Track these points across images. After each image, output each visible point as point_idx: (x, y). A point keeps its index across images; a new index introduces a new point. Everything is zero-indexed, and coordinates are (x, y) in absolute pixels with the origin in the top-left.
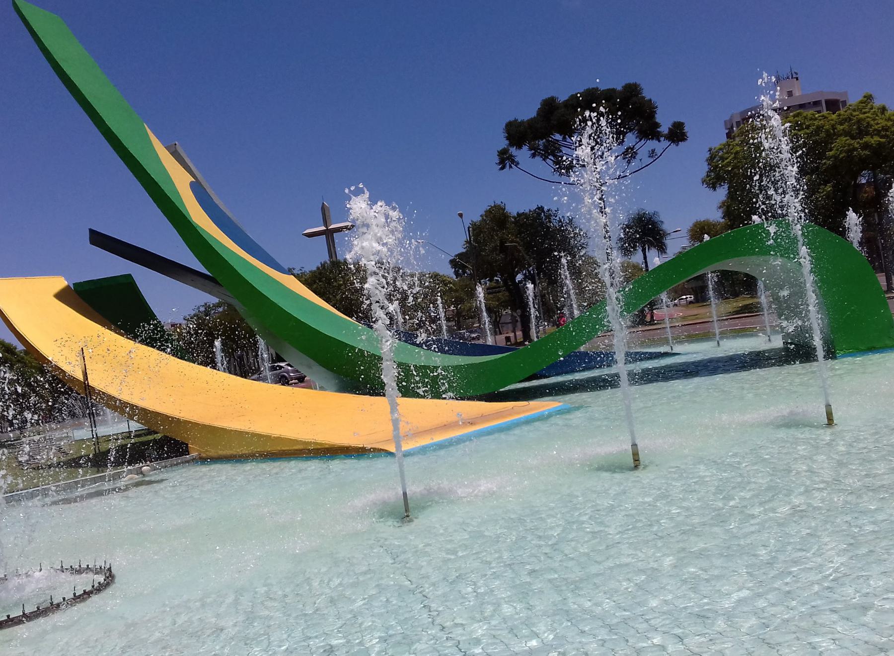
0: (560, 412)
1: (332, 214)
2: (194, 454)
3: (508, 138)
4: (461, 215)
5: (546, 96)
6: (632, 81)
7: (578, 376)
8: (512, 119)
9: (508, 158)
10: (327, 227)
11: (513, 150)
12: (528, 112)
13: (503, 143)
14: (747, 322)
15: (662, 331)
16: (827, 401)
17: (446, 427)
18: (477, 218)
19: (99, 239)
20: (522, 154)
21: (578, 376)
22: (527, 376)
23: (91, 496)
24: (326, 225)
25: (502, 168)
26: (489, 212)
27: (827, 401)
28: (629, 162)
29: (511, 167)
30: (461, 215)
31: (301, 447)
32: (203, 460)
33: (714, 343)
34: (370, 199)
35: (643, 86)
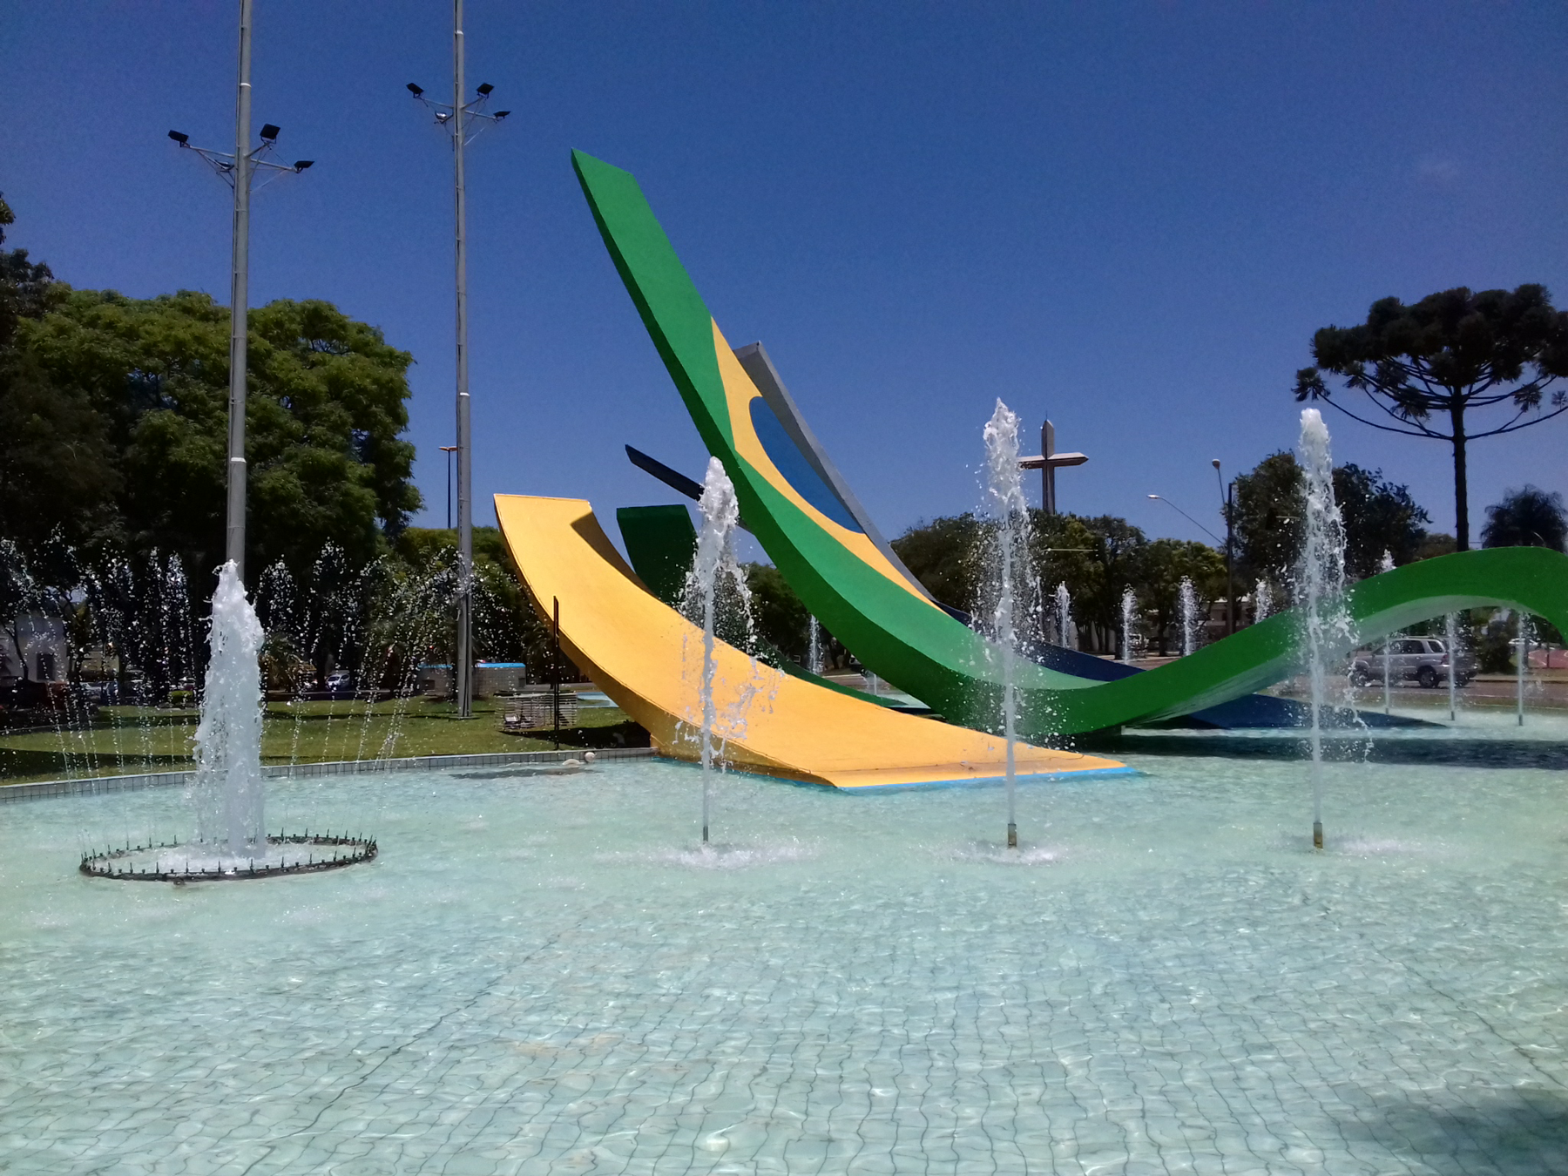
0: (1114, 776)
1: (1057, 438)
2: (654, 748)
3: (1317, 354)
4: (1216, 465)
5: (1381, 295)
6: (1532, 281)
7: (1253, 734)
8: (1327, 326)
9: (1311, 384)
10: (1046, 455)
11: (1324, 375)
12: (1353, 316)
13: (1310, 361)
14: (446, 706)
15: (1507, 686)
16: (1012, 818)
17: (936, 768)
18: (1248, 471)
19: (637, 457)
20: (1334, 381)
21: (1253, 734)
22: (1129, 717)
23: (518, 774)
24: (1045, 454)
25: (1301, 399)
26: (1270, 464)
27: (1012, 818)
28: (1525, 409)
29: (1315, 397)
30: (1216, 465)
31: (751, 760)
32: (664, 757)
33: (1512, 718)
34: (411, 509)
35: (1550, 289)
